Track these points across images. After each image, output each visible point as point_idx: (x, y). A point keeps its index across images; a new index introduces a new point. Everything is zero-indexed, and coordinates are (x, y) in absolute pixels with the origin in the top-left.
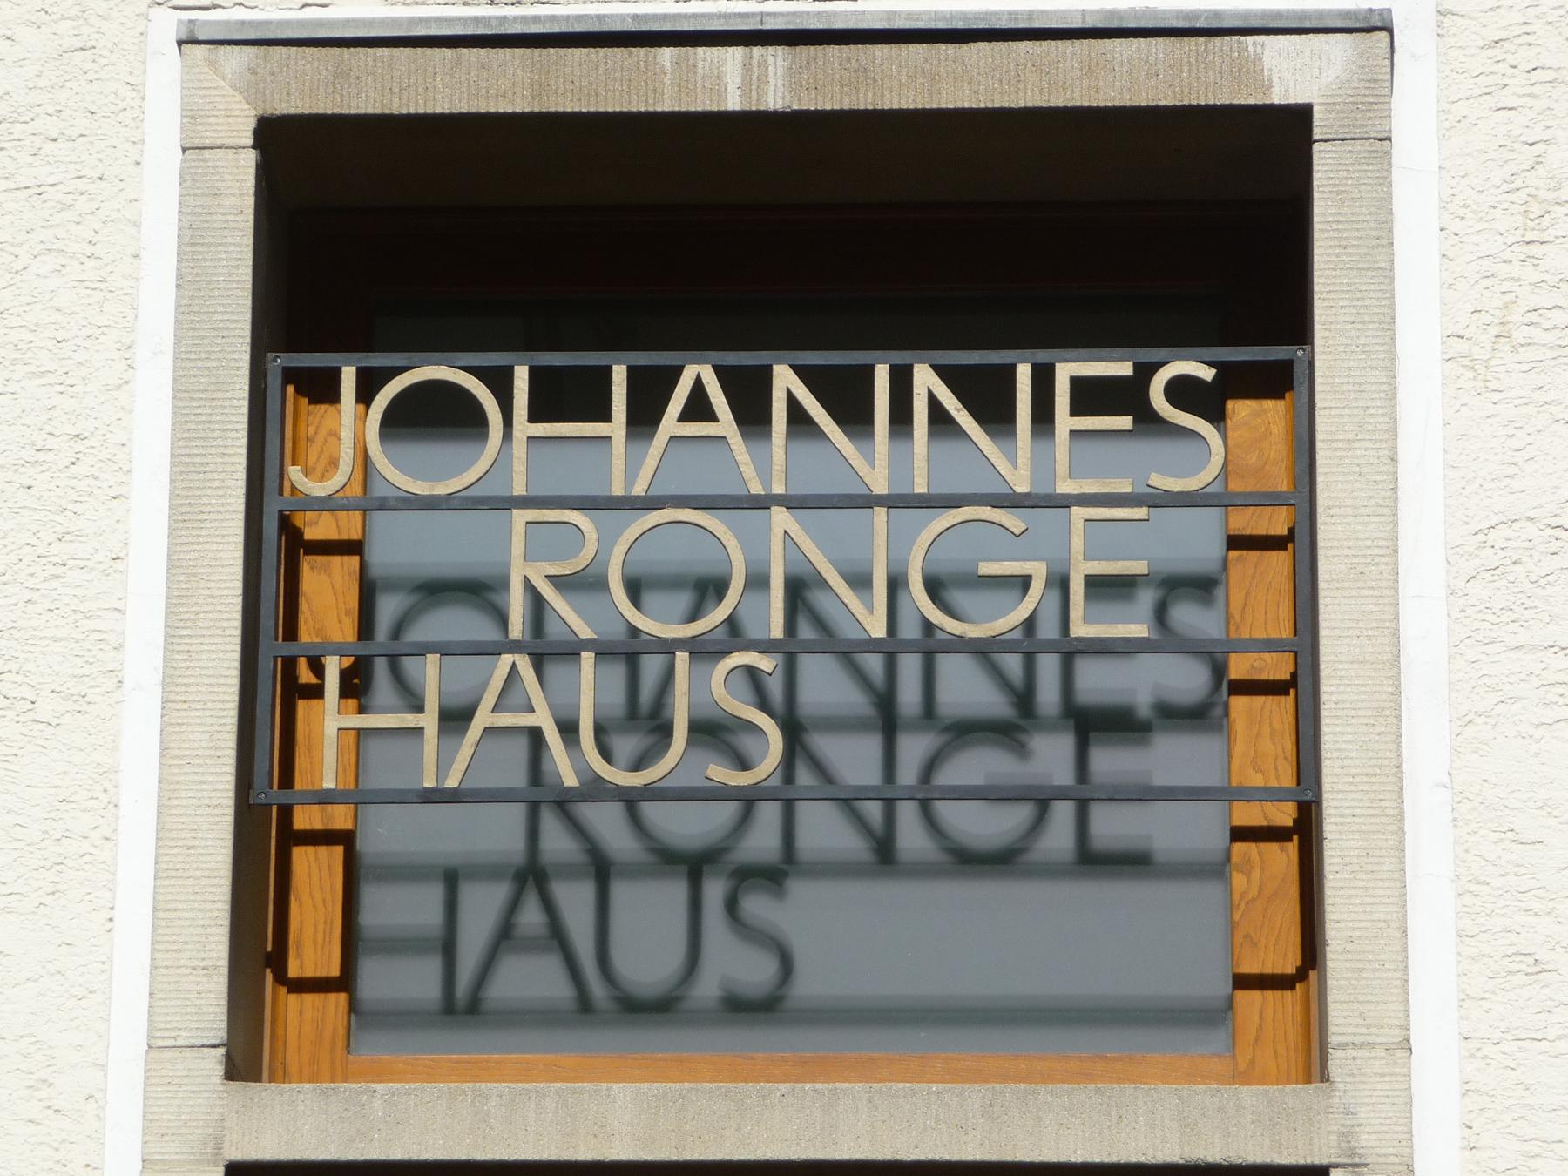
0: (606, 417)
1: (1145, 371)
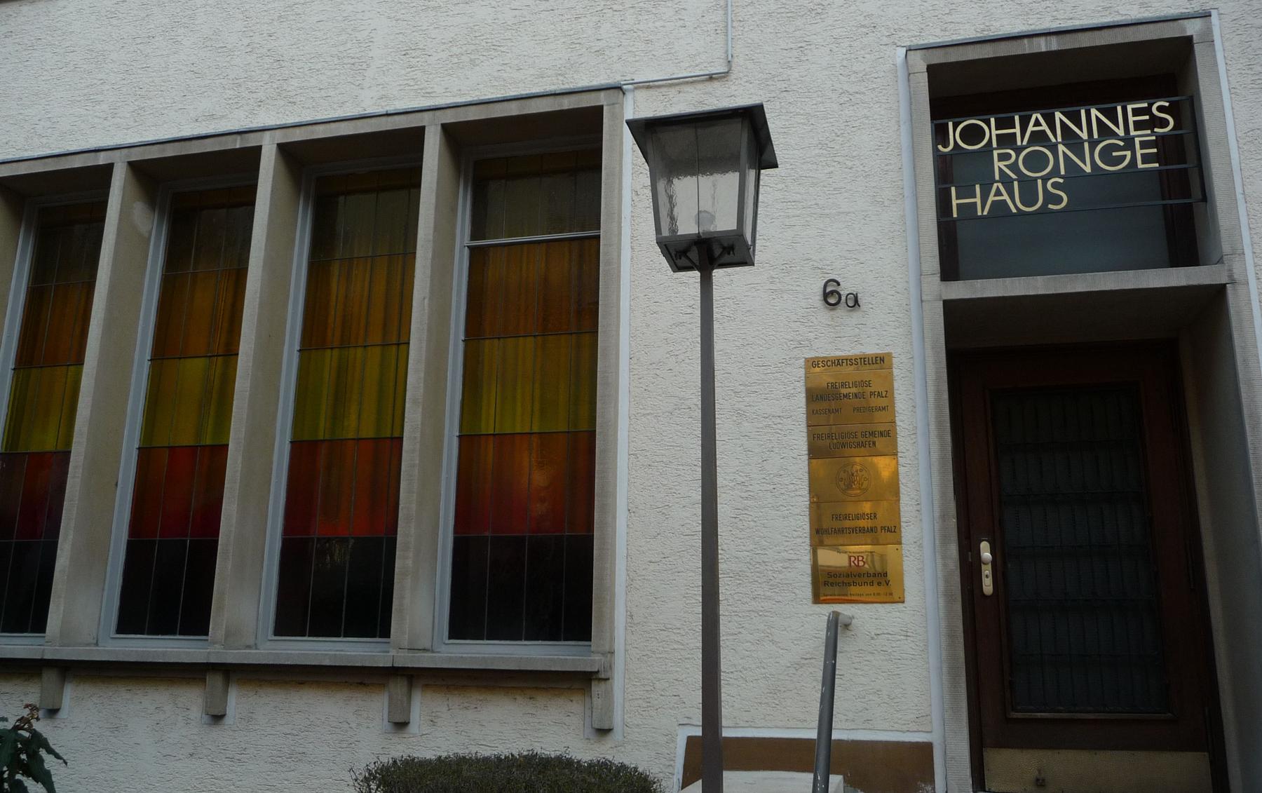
0: (1014, 127)
1: (1151, 105)
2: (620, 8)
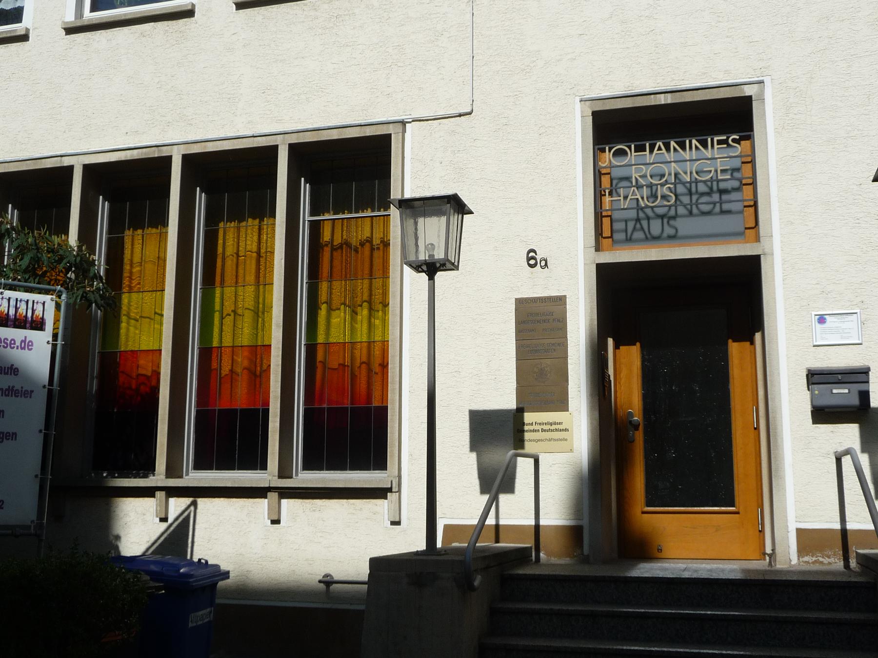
1: (728, 138)
2: (402, 65)
